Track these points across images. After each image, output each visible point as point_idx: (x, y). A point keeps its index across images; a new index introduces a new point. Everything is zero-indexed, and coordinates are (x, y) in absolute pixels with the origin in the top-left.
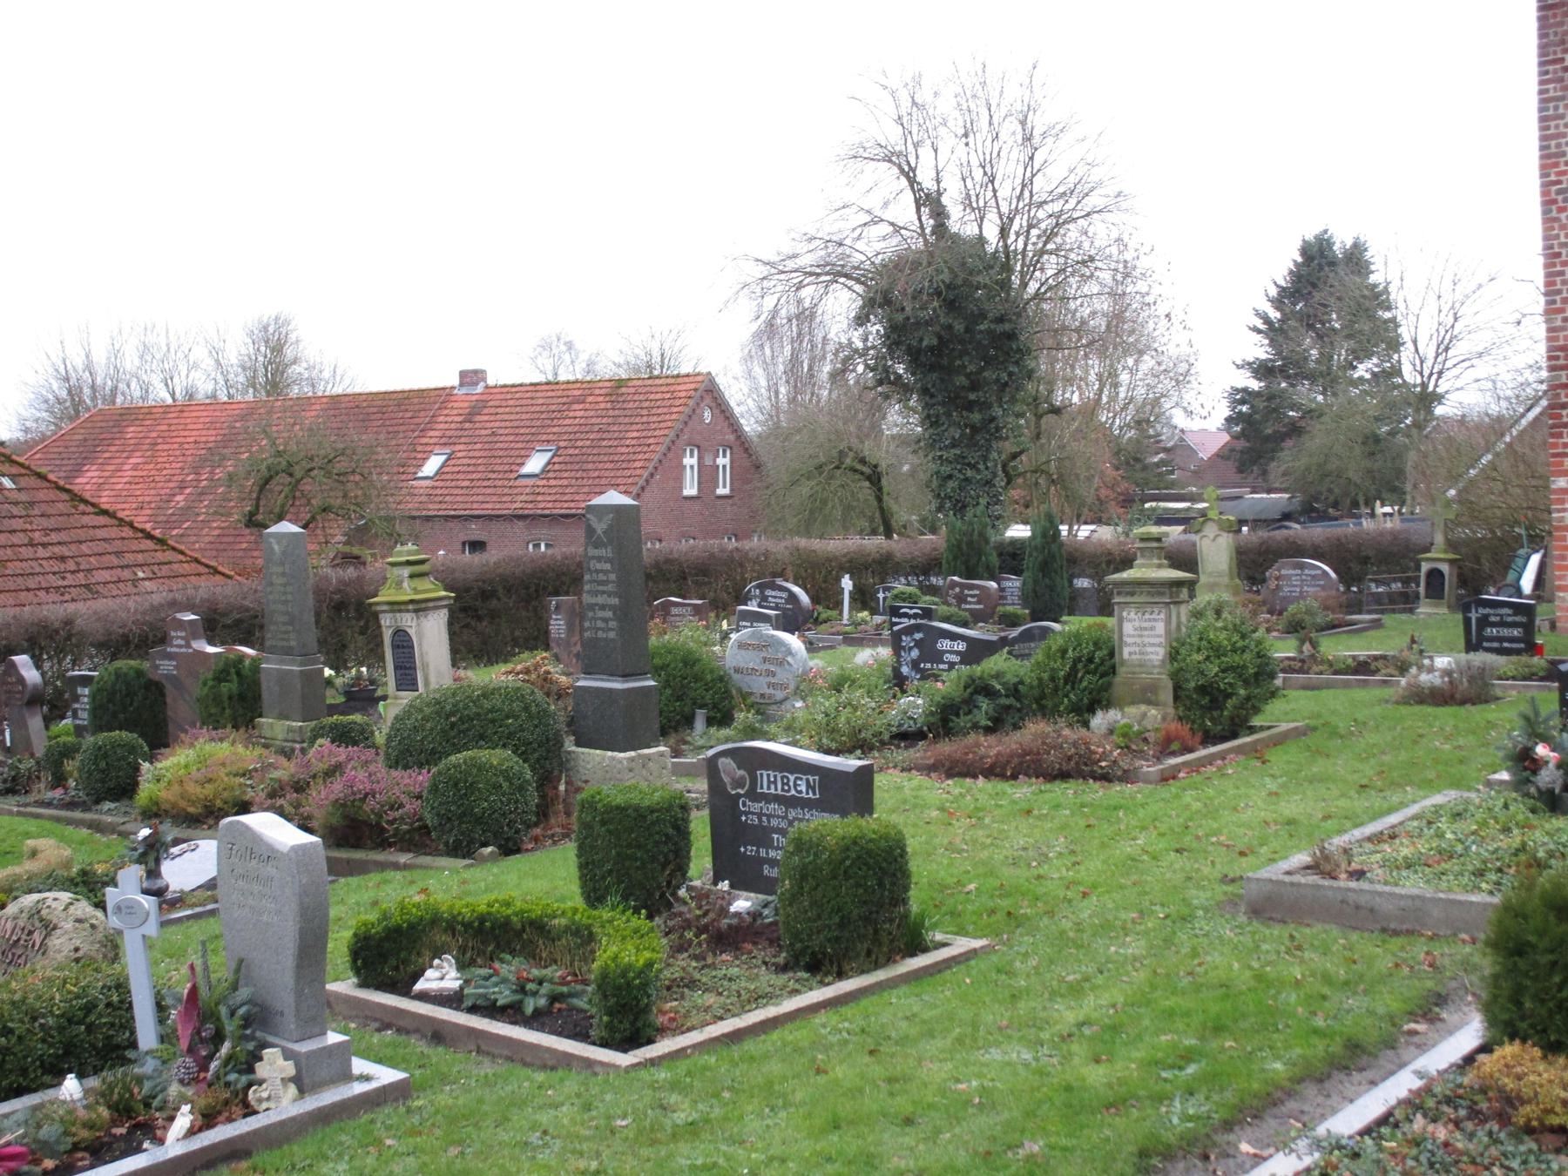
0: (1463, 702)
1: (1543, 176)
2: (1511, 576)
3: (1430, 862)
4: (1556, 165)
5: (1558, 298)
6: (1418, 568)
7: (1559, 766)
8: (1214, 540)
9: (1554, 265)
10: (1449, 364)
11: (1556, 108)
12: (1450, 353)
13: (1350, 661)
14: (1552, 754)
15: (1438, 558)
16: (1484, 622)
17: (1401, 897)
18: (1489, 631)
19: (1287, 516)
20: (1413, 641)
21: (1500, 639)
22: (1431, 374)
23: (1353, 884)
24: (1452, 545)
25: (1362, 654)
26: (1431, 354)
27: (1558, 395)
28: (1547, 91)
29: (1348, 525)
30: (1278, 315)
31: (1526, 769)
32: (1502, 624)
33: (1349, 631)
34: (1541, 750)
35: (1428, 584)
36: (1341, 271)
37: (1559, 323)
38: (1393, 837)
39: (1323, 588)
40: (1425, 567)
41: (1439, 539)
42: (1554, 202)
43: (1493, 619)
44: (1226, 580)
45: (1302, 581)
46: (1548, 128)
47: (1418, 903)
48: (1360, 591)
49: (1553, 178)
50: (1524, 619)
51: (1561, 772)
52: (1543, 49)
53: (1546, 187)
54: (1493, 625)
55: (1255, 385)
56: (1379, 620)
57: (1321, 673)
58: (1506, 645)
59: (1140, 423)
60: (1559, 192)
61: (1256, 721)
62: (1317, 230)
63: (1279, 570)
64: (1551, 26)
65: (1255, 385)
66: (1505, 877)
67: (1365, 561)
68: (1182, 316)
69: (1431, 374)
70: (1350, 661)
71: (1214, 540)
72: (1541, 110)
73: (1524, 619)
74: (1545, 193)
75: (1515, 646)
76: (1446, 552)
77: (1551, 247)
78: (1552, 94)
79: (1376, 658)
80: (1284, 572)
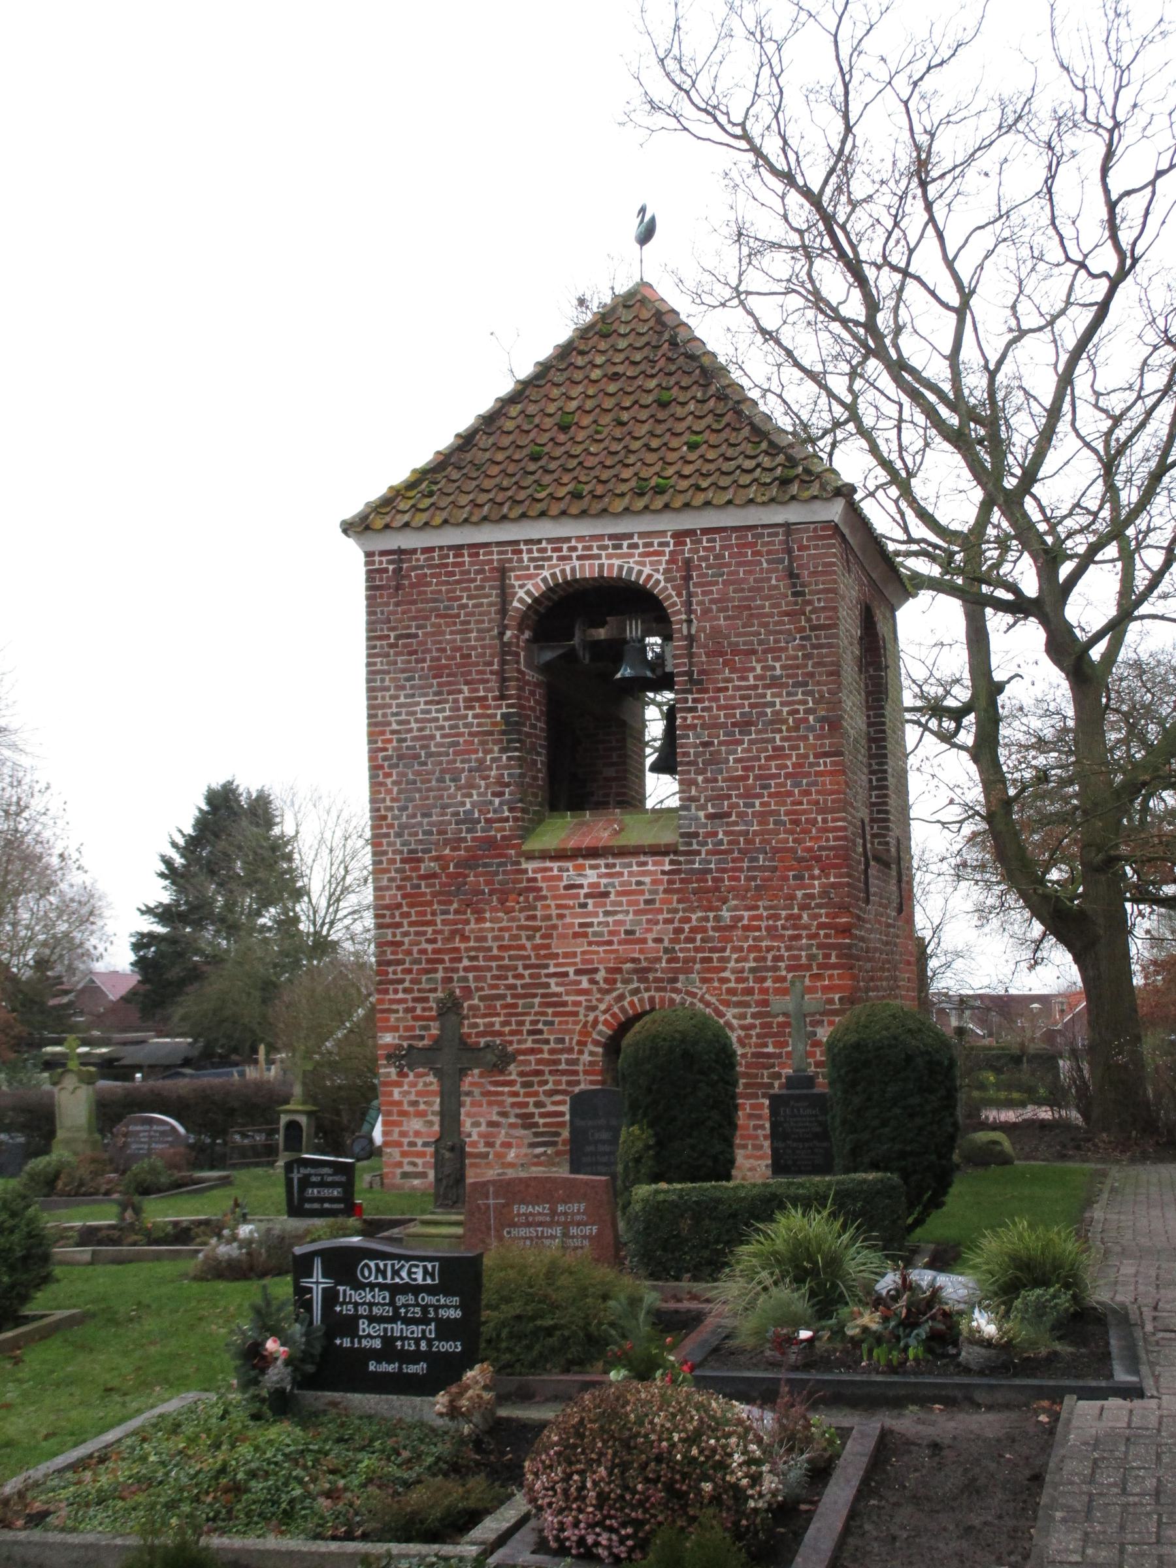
0: (263, 1275)
1: (370, 742)
2: (366, 1127)
3: (125, 1494)
4: (383, 733)
5: (384, 858)
6: (278, 1121)
7: (287, 1363)
8: (73, 1092)
9: (381, 827)
10: (340, 915)
11: (383, 680)
12: (342, 904)
13: (169, 1228)
14: (282, 1349)
15: (296, 1111)
16: (305, 1182)
17: (74, 1547)
18: (313, 1192)
19: (187, 1062)
20: (237, 1205)
21: (322, 1200)
22: (323, 924)
23: (36, 1535)
24: (309, 1097)
25: (186, 1218)
26: (323, 903)
27: (384, 952)
28: (375, 664)
29: (231, 1074)
30: (182, 861)
31: (254, 1367)
32: (322, 1184)
33: (189, 1192)
34: (271, 1345)
35: (287, 1137)
36: (244, 823)
37: (385, 883)
38: (102, 1460)
39: (172, 1144)
40: (284, 1119)
41: (298, 1090)
42: (381, 767)
43: (314, 1179)
44: (84, 1135)
45: (151, 1137)
46: (376, 698)
47: (91, 1554)
48: (225, 1143)
49: (380, 745)
50: (344, 1179)
51: (290, 1369)
52: (371, 626)
53: (373, 753)
54: (315, 1185)
55: (160, 929)
56: (227, 1177)
57: (135, 1244)
58: (326, 1205)
59: (41, 964)
60: (385, 759)
61: (27, 1311)
62: (222, 781)
63: (127, 1126)
64: (380, 605)
65: (160, 929)
66: (202, 1507)
67: (231, 1112)
68: (74, 857)
69: (323, 924)
70: (169, 1228)
71: (73, 1092)
72: (369, 681)
73: (344, 1179)
74: (372, 759)
75: (335, 1206)
76: (304, 1103)
77: (378, 810)
78: (379, 667)
79: (200, 1223)
80: (131, 1128)
